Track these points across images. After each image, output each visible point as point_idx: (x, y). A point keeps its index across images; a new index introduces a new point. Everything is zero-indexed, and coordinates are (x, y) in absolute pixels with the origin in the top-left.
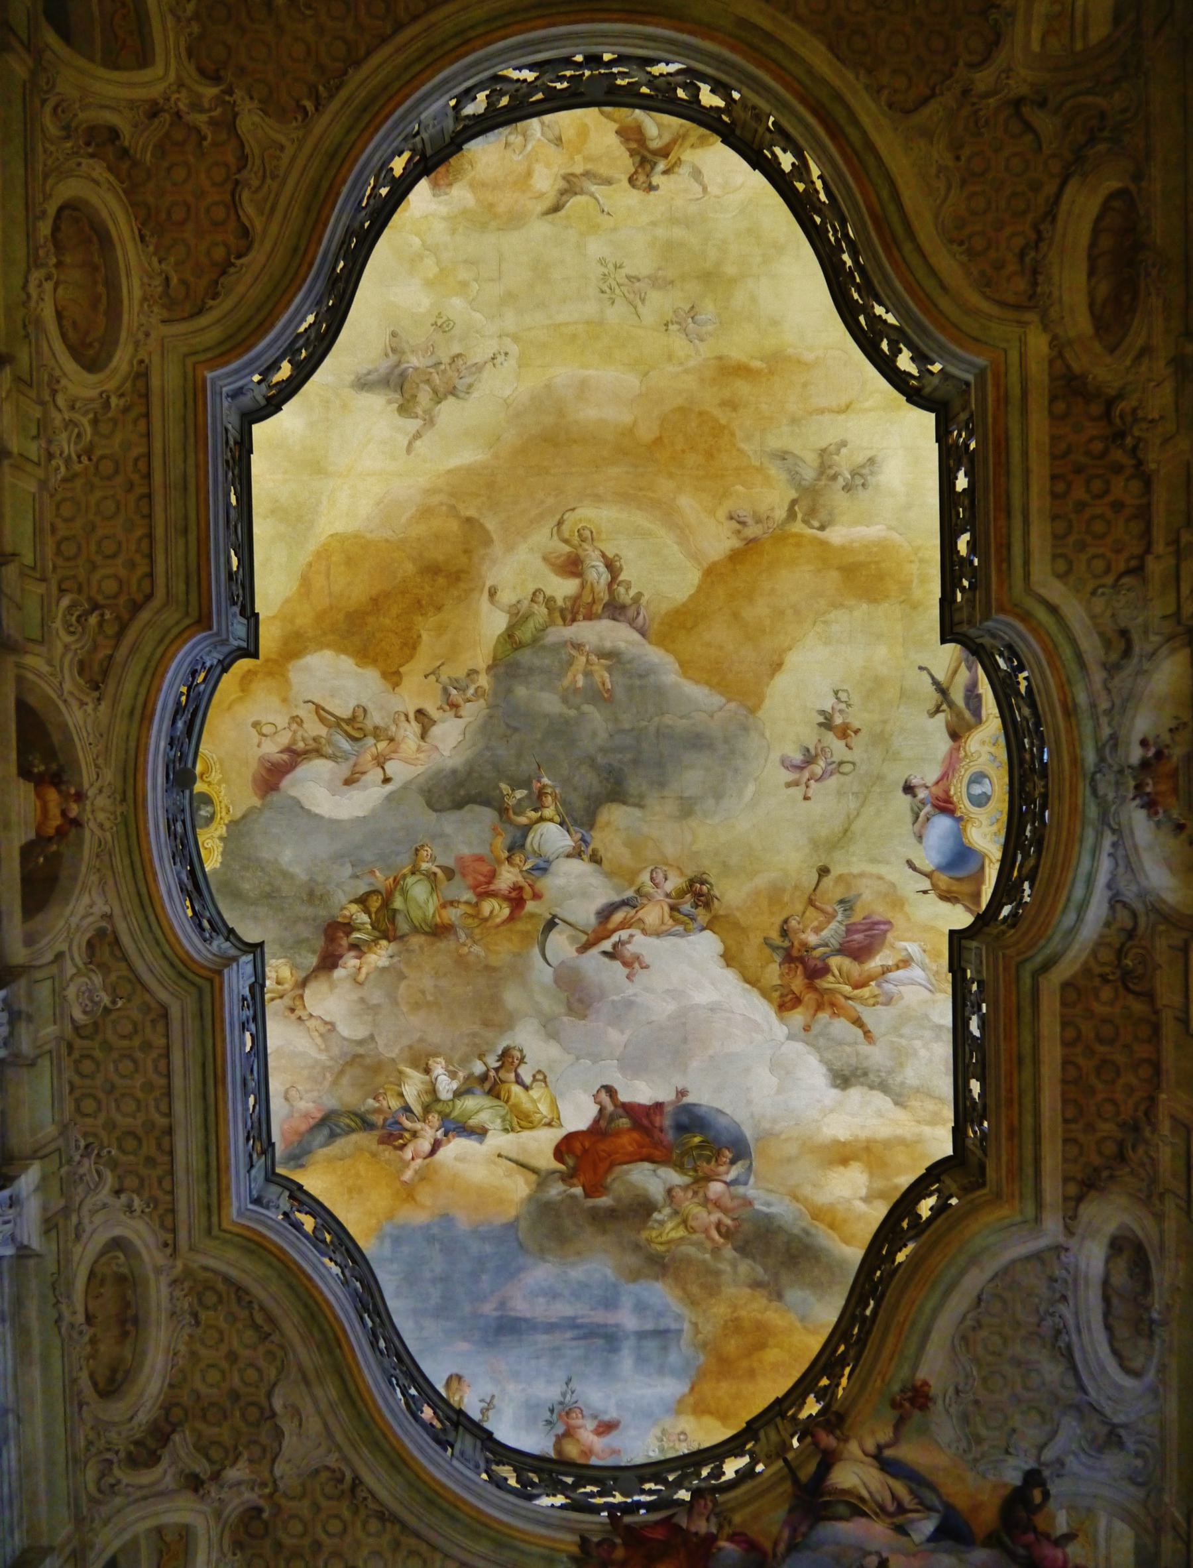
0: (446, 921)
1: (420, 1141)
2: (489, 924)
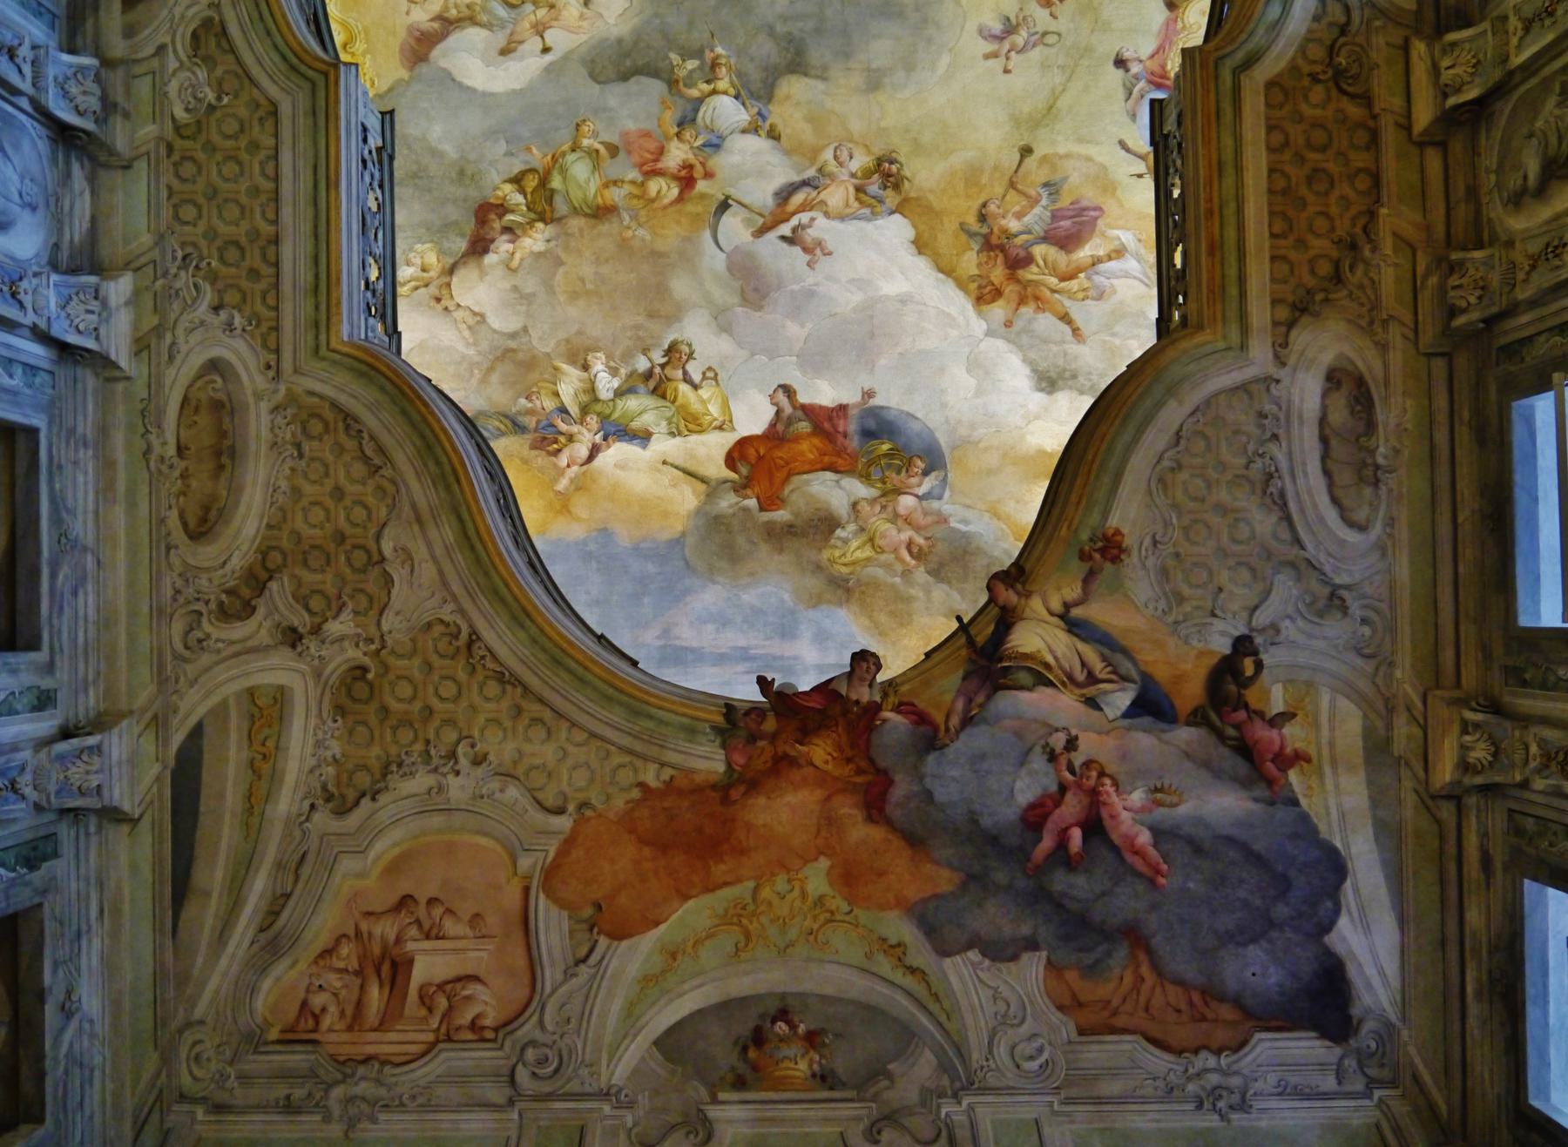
0: (609, 202)
1: (576, 446)
2: (656, 205)
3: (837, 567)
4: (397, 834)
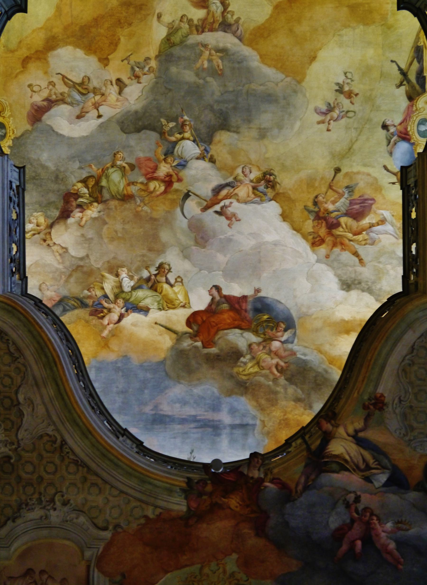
0: (130, 193)
1: (112, 314)
3: (240, 376)
4: (25, 538)
